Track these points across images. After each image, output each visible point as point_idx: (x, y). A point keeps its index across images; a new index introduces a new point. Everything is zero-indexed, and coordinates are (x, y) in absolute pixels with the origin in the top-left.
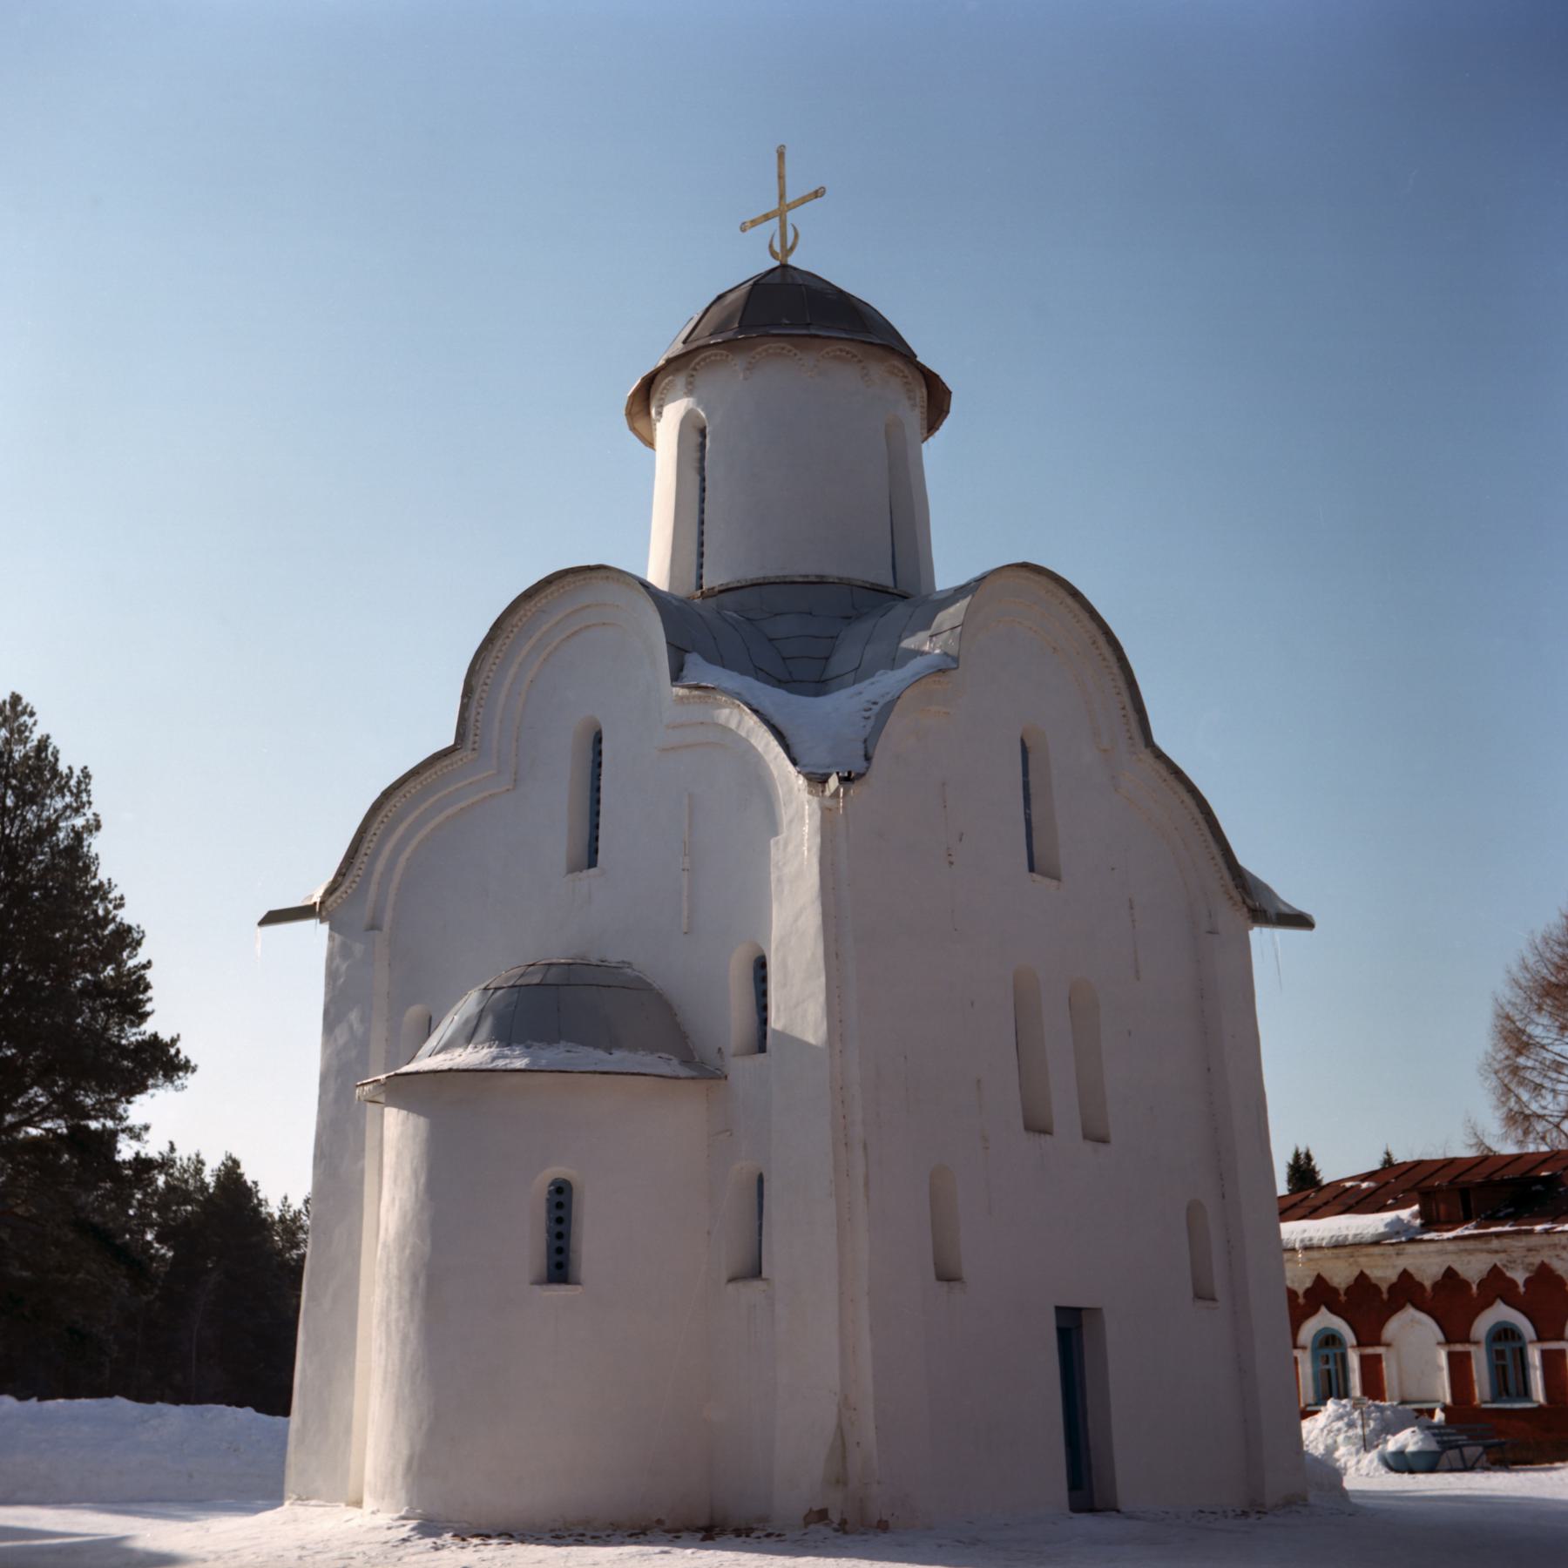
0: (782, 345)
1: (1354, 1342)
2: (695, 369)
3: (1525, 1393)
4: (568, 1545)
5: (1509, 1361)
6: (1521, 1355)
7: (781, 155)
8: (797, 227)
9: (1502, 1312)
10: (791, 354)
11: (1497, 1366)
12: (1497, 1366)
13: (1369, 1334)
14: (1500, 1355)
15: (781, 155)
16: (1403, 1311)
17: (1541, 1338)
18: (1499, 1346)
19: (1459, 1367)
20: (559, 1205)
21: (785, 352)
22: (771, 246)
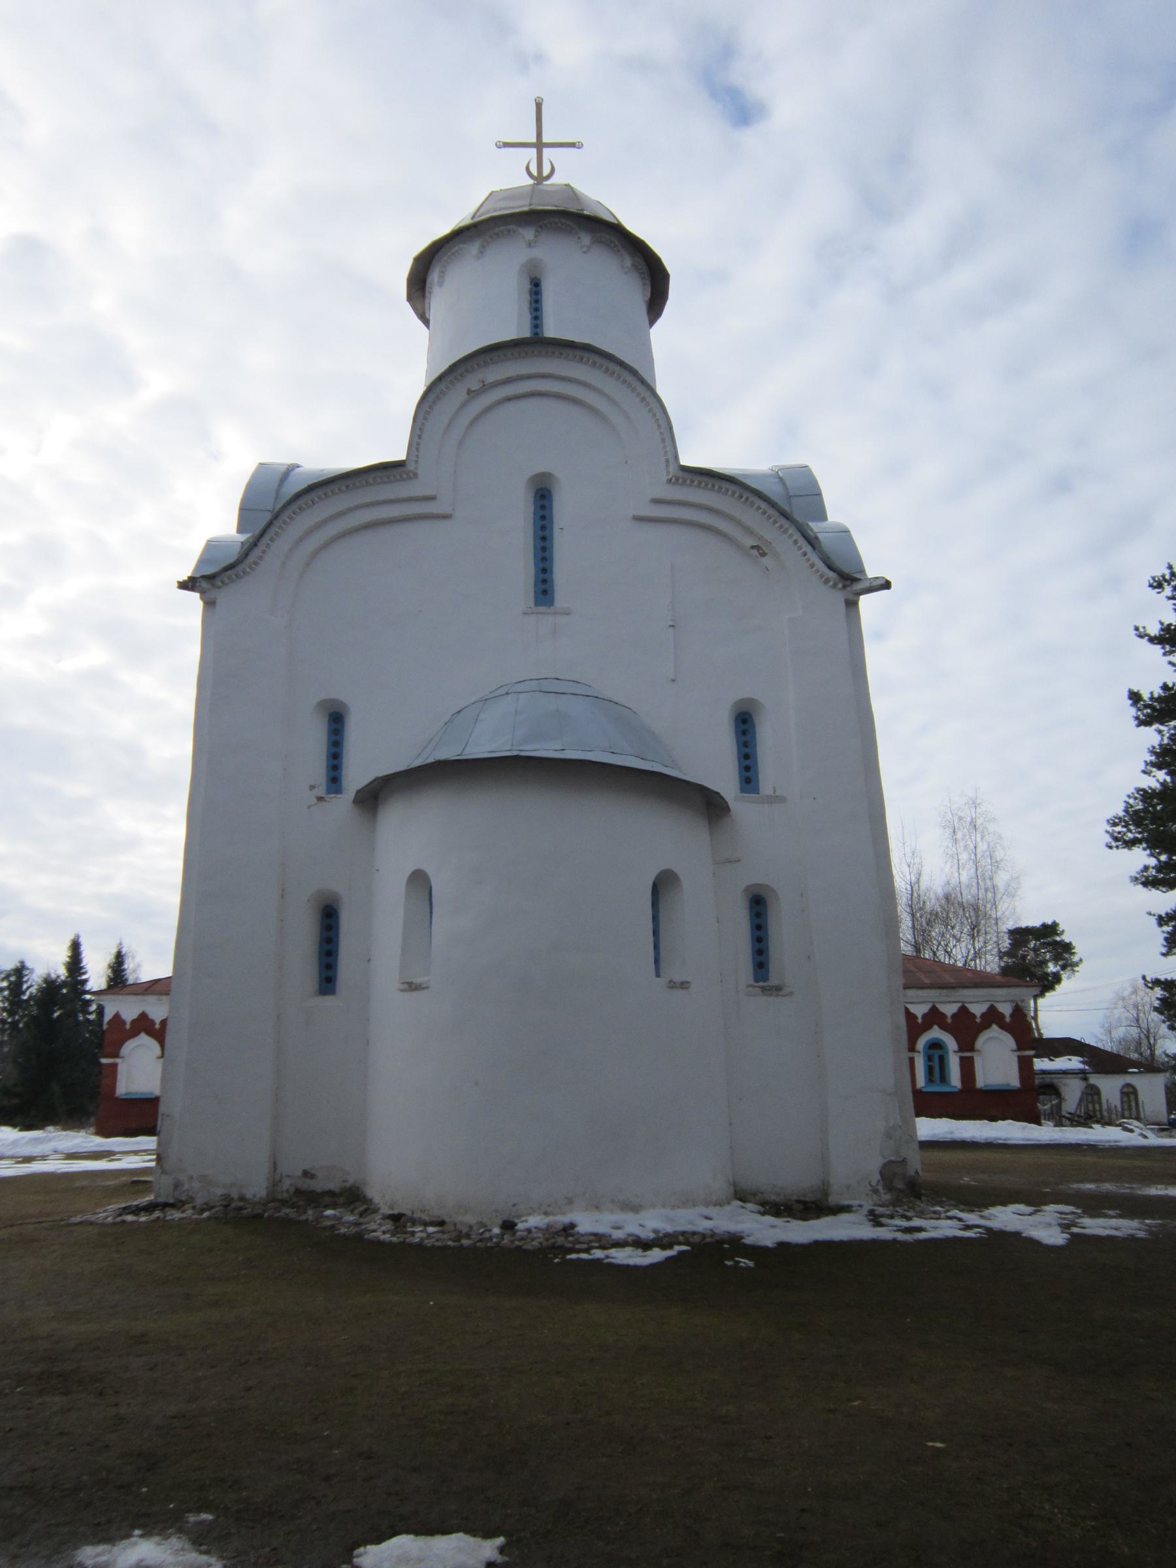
2: (541, 227)
3: (944, 1078)
5: (936, 1064)
7: (539, 106)
9: (936, 1033)
13: (967, 1044)
15: (539, 106)
18: (932, 1052)
20: (543, 528)
22: (527, 168)
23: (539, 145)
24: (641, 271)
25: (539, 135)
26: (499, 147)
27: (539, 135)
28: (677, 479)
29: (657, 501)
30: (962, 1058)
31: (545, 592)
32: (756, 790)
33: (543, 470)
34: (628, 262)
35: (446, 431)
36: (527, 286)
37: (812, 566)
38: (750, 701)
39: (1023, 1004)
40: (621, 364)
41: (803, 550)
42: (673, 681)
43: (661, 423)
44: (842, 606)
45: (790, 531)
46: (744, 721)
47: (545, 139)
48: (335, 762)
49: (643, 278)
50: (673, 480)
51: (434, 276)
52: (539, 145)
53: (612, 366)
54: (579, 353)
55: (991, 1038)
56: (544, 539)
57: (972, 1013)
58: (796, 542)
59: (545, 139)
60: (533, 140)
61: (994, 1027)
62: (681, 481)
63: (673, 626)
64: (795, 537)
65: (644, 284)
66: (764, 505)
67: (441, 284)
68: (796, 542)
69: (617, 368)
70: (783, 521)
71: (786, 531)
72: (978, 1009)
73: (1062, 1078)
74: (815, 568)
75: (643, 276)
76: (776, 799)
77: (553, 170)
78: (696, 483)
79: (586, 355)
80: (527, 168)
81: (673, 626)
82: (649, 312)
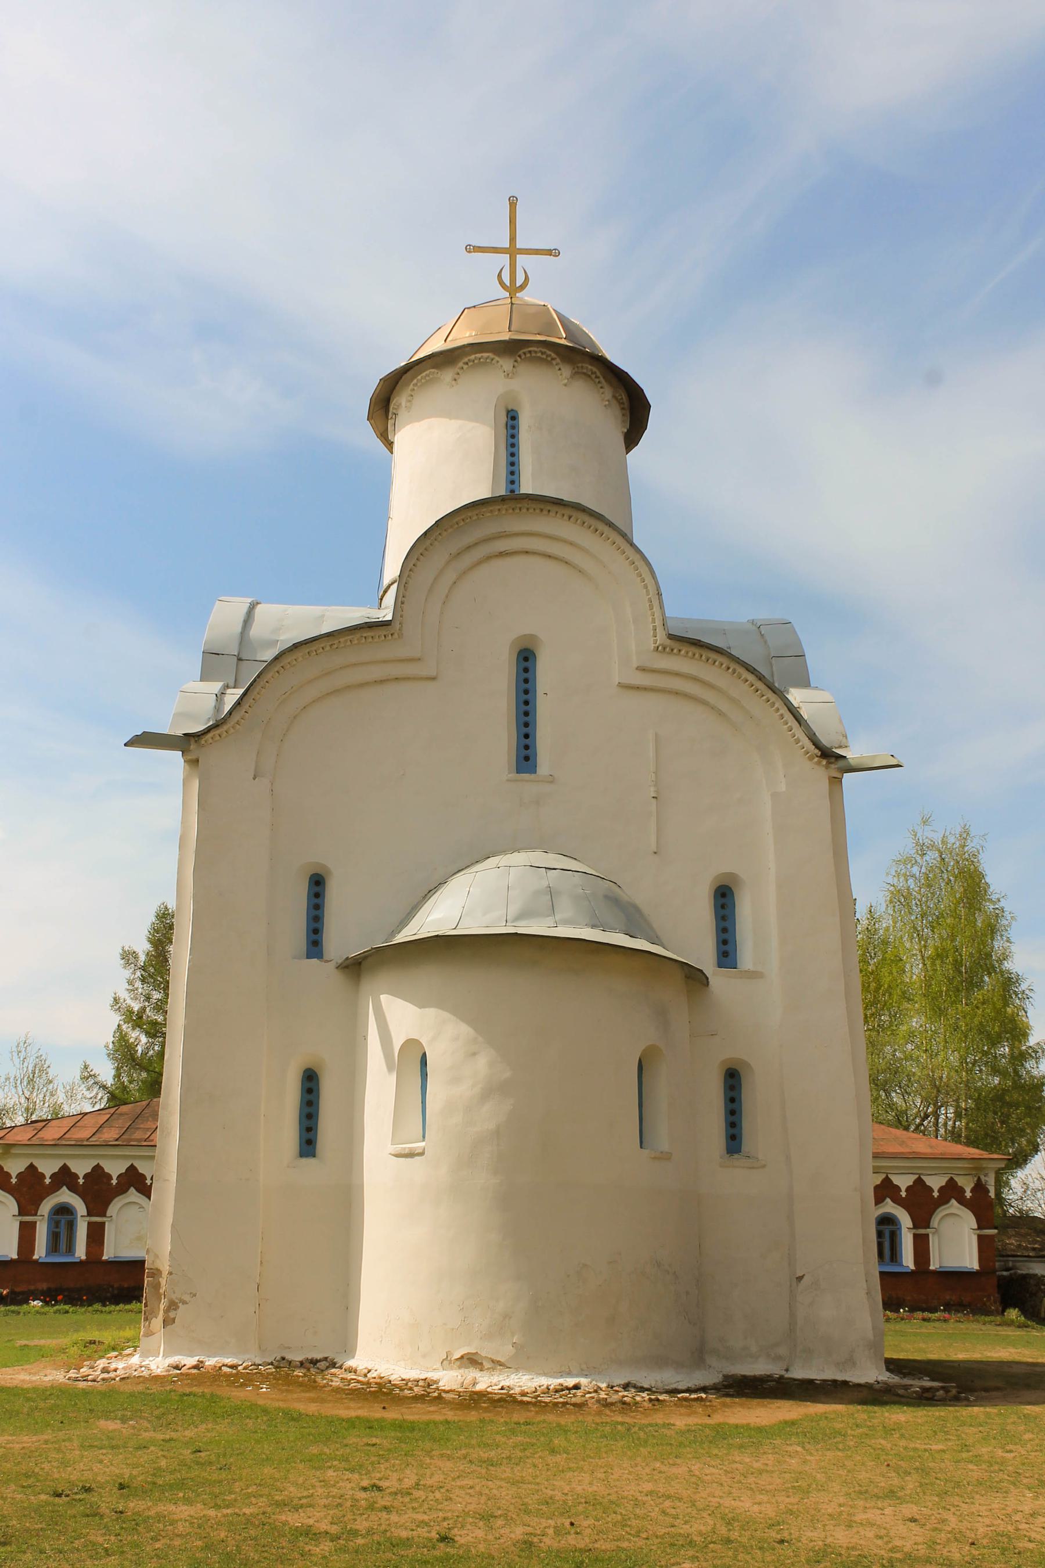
0: (594, 369)
1: (911, 1225)
3: (70, 1249)
4: (851, 1402)
6: (71, 1226)
8: (527, 272)
9: (65, 1196)
10: (597, 380)
11: (53, 1232)
12: (53, 1232)
13: (922, 1220)
14: (57, 1224)
16: (124, 1195)
17: (90, 1214)
18: (882, 1227)
19: (27, 1233)
21: (593, 376)
22: (499, 275)
23: (513, 251)
24: (622, 406)
25: (513, 239)
26: (470, 252)
27: (513, 239)
28: (664, 649)
29: (642, 669)
30: (915, 1236)
31: (527, 758)
32: (533, 770)
33: (527, 632)
34: (608, 392)
35: (430, 590)
36: (503, 418)
37: (798, 741)
38: (732, 876)
39: (986, 1179)
40: (610, 525)
41: (789, 724)
42: (655, 853)
43: (649, 588)
44: (826, 783)
45: (781, 711)
46: (526, 659)
47: (519, 245)
48: (316, 925)
49: (623, 409)
50: (660, 648)
51: (401, 400)
52: (513, 251)
53: (601, 527)
54: (568, 512)
55: (947, 1215)
56: (527, 747)
57: (929, 1186)
58: (782, 716)
59: (519, 245)
60: (506, 244)
61: (953, 1202)
62: (668, 649)
63: (656, 798)
64: (781, 711)
65: (623, 421)
66: (751, 678)
67: (408, 408)
68: (782, 716)
69: (606, 529)
70: (770, 694)
71: (773, 704)
72: (936, 1183)
73: (1026, 1261)
74: (800, 744)
75: (624, 411)
76: (754, 975)
77: (527, 278)
78: (683, 652)
79: (576, 514)
80: (499, 275)
81: (656, 798)
82: (626, 449)
